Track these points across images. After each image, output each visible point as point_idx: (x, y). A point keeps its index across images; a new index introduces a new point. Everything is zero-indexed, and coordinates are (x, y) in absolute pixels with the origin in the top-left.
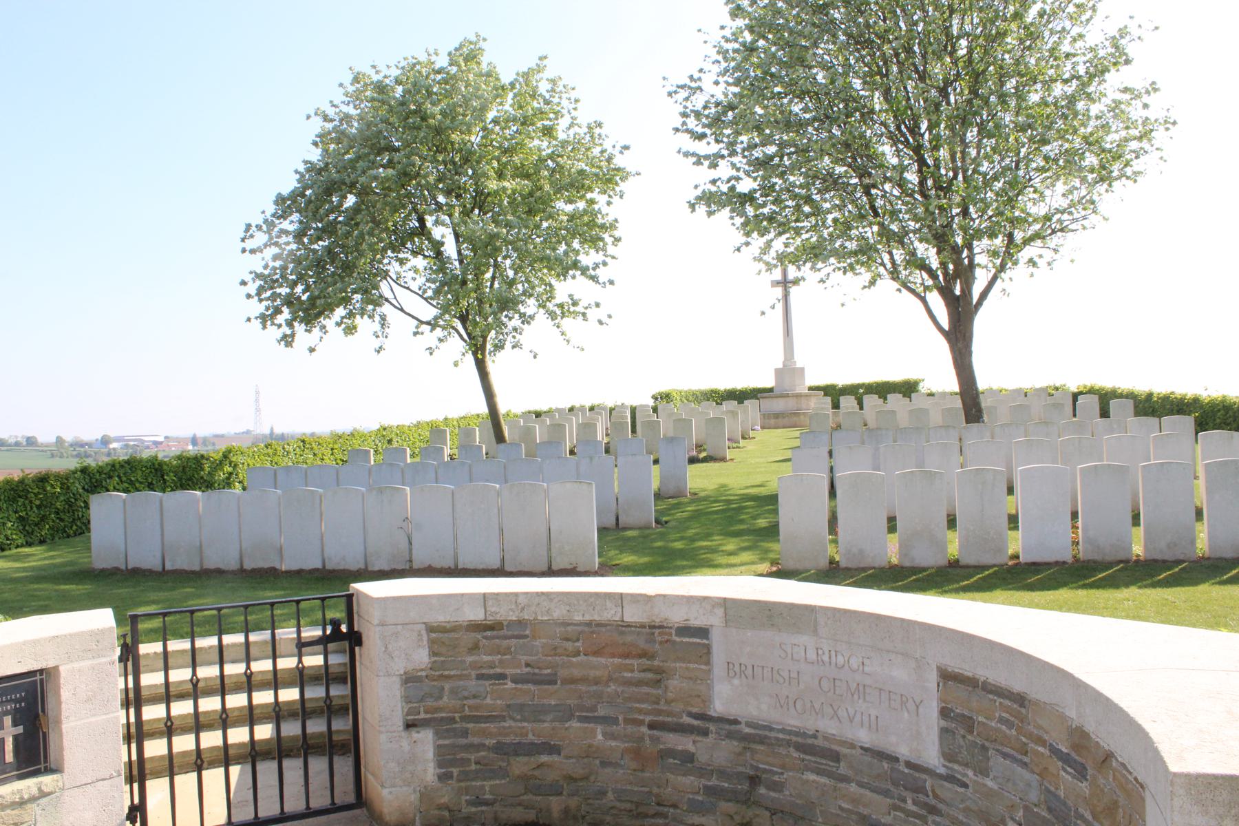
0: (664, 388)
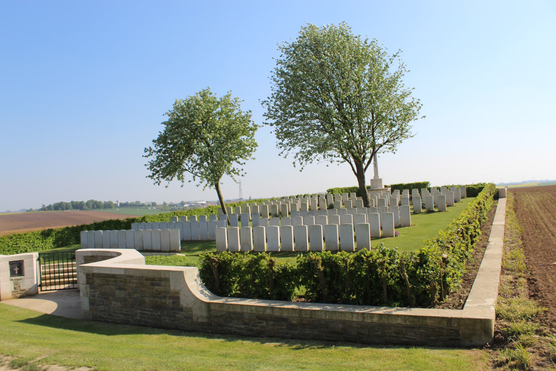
0: (332, 188)
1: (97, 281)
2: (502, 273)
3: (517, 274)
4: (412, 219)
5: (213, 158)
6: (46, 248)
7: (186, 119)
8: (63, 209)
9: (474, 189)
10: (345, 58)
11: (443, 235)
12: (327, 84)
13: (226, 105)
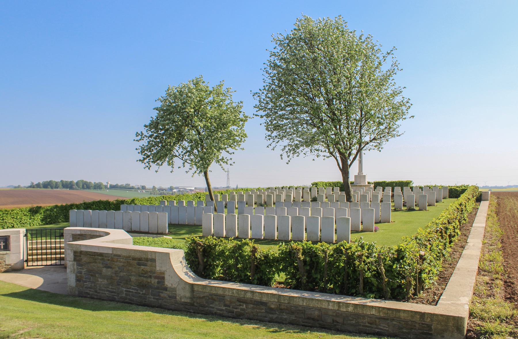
0: (316, 181)
1: (85, 259)
2: (479, 273)
3: (494, 276)
4: (393, 216)
5: (203, 146)
6: (34, 225)
7: (178, 106)
8: (52, 188)
9: (456, 190)
10: (339, 54)
11: (422, 233)
12: (319, 79)
13: (218, 95)
